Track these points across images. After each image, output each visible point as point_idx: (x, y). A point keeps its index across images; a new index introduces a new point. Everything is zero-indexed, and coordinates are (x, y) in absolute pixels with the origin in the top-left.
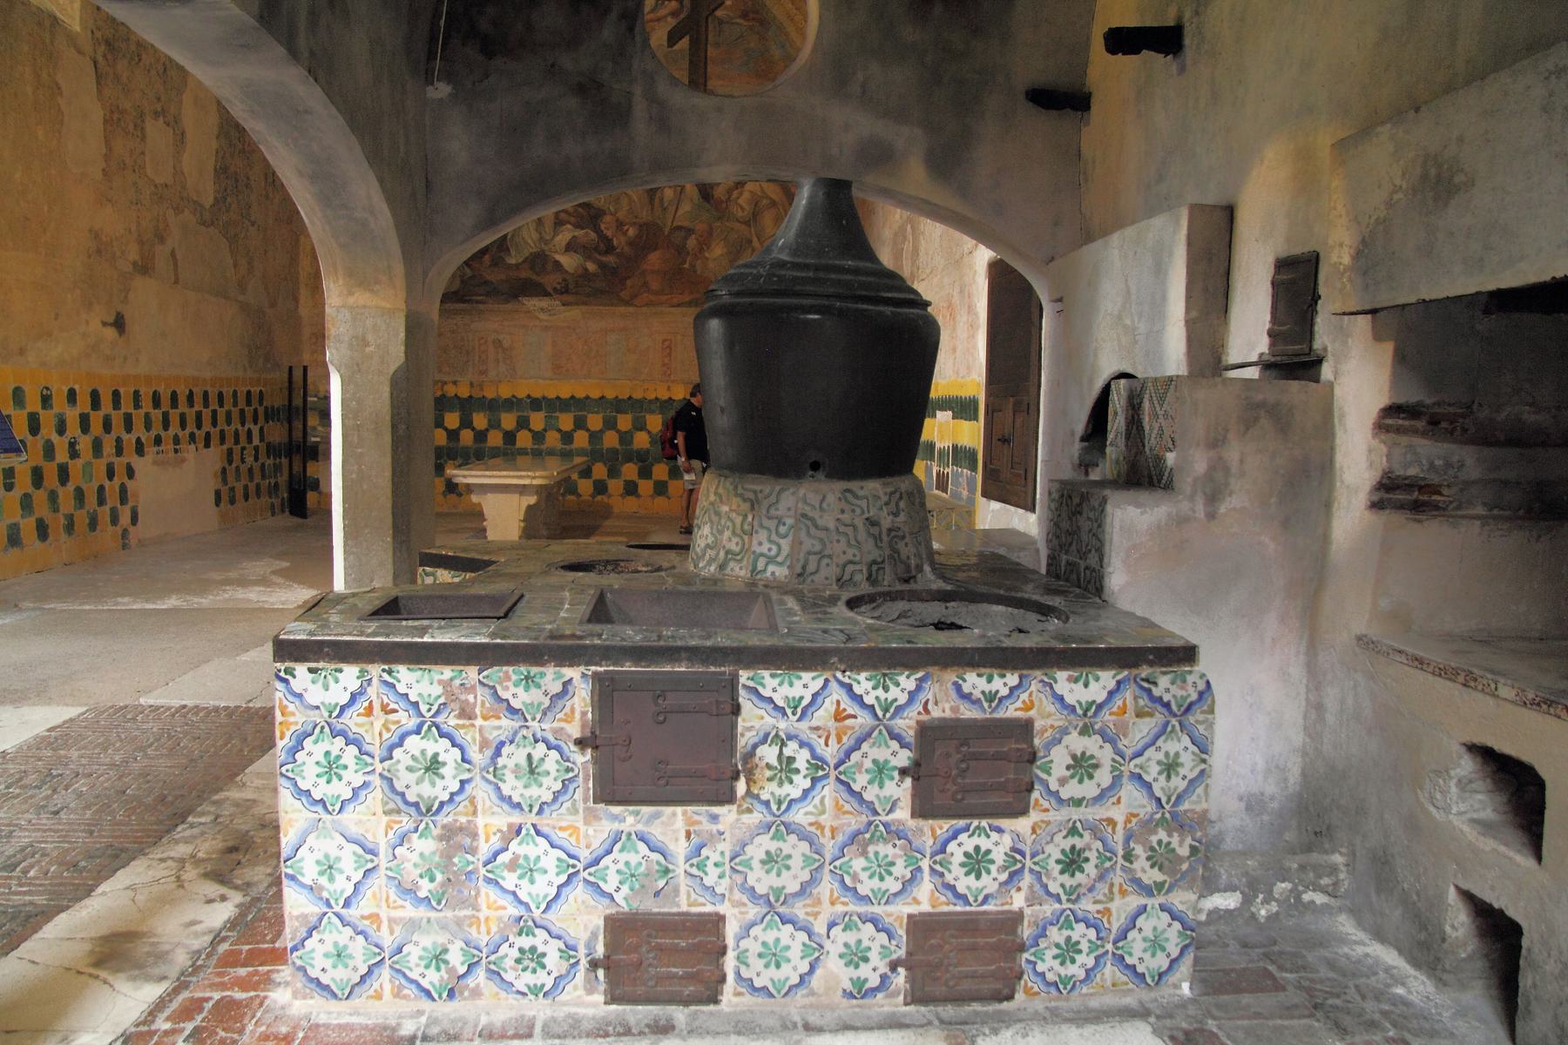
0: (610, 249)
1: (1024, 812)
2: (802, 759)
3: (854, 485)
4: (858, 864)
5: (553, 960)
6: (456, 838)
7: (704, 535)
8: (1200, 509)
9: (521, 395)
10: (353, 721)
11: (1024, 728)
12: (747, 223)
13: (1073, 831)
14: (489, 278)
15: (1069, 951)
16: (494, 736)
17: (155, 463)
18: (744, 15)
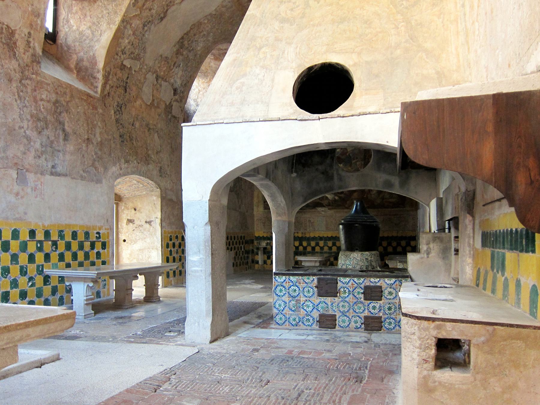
1: (381, 300)
2: (347, 291)
3: (363, 253)
4: (356, 307)
5: (311, 321)
6: (298, 301)
7: (339, 261)
8: (425, 256)
9: (317, 236)
10: (284, 284)
11: (381, 287)
13: (389, 304)
15: (390, 323)
16: (304, 286)
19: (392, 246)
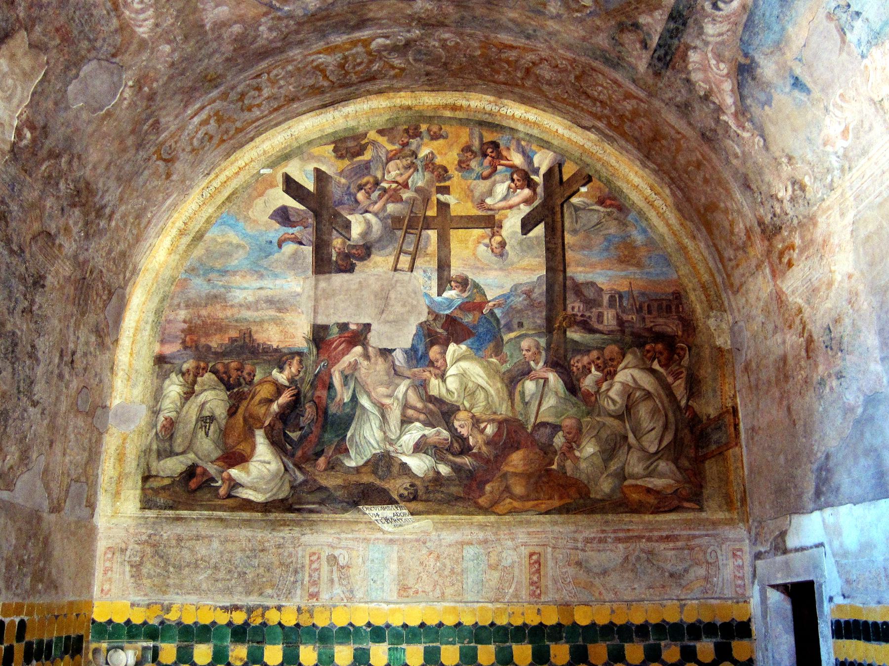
0: (465, 449)
9: (360, 622)
12: (620, 417)
14: (324, 482)
18: (601, 202)
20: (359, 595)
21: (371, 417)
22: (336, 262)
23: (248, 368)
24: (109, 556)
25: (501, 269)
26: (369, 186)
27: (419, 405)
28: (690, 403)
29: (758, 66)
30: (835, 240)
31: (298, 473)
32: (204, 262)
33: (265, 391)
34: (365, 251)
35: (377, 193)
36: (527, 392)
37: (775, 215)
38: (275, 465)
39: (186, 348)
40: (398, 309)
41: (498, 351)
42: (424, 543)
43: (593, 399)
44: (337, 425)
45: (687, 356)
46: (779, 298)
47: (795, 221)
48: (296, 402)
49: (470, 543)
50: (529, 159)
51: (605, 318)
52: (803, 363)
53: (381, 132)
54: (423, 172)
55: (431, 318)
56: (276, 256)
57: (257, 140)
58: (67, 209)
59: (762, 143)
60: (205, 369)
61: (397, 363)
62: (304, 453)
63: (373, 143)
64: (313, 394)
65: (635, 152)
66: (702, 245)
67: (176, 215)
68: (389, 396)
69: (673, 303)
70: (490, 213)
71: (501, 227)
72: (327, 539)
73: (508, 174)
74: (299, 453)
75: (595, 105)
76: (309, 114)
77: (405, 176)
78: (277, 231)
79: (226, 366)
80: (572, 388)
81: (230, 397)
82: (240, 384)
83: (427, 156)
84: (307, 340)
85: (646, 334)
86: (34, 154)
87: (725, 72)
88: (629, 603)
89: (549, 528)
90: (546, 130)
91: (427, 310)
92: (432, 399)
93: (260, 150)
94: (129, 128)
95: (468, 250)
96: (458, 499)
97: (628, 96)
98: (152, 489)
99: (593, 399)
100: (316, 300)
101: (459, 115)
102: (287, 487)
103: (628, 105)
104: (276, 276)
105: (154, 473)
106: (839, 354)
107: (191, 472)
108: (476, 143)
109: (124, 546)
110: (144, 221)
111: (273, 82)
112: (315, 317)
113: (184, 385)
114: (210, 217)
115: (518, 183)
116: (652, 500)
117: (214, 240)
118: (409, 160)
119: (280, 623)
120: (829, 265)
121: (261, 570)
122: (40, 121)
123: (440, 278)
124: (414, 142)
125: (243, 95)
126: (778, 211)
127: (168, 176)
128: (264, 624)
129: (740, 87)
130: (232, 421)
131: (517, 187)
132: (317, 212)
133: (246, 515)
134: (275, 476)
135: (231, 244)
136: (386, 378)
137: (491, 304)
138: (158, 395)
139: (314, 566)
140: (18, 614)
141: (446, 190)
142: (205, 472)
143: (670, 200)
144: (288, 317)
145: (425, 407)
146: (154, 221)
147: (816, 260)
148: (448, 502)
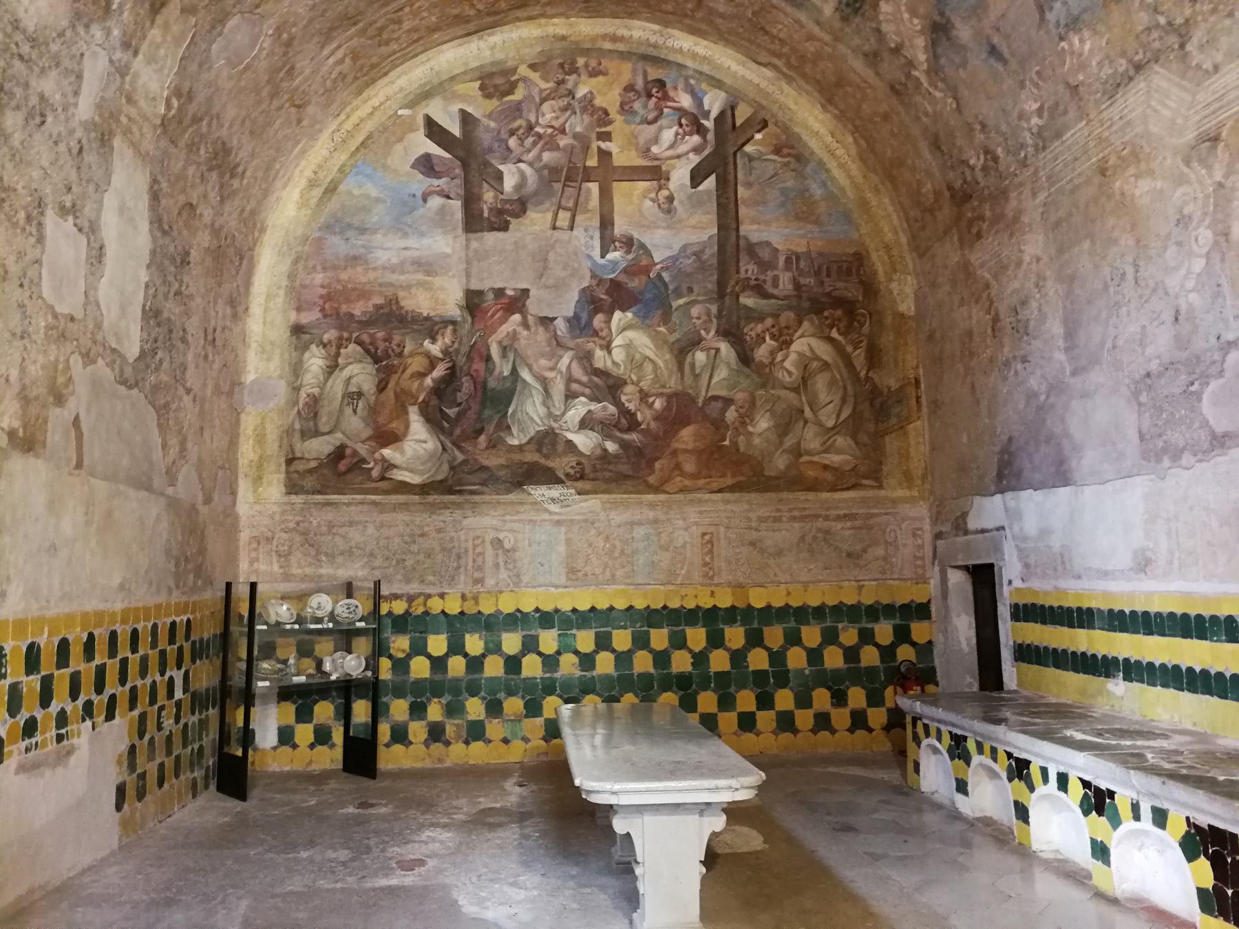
0: (633, 425)
9: (528, 608)
12: (796, 390)
14: (486, 463)
17: (22, 769)
18: (777, 151)
19: (840, 645)
20: (525, 579)
21: (534, 392)
22: (488, 219)
23: (397, 338)
24: (255, 545)
25: (668, 227)
26: (521, 131)
27: (584, 379)
28: (870, 374)
29: (953, 27)
30: (1025, 219)
31: (457, 453)
32: (336, 220)
33: (417, 364)
34: (520, 206)
35: (531, 139)
36: (697, 364)
37: (965, 182)
38: (432, 444)
39: (325, 316)
40: (558, 272)
41: (666, 319)
42: (593, 523)
43: (767, 370)
44: (498, 399)
45: (868, 323)
46: (966, 269)
47: (986, 192)
48: (452, 376)
49: (640, 523)
50: (699, 102)
51: (781, 282)
52: (988, 341)
53: (533, 67)
54: (582, 114)
55: (594, 283)
56: (421, 211)
57: (392, 74)
58: (206, 174)
59: (954, 106)
60: (349, 340)
61: (559, 333)
62: (463, 431)
63: (524, 79)
64: (469, 368)
65: (816, 94)
66: (886, 200)
67: (303, 163)
68: (552, 369)
69: (854, 265)
70: (656, 163)
71: (668, 179)
72: (486, 520)
73: (676, 118)
74: (458, 431)
75: (773, 42)
76: (449, 44)
77: (561, 120)
78: (420, 183)
79: (372, 336)
80: (745, 358)
81: (378, 370)
82: (388, 357)
83: (585, 96)
84: (461, 308)
85: (824, 300)
86: (180, 122)
87: (919, 27)
88: (806, 585)
89: (722, 507)
90: (718, 66)
91: (589, 274)
92: (598, 372)
93: (396, 87)
94: (266, 78)
95: (633, 204)
96: (627, 477)
97: (811, 37)
98: (297, 472)
99: (767, 370)
100: (468, 262)
101: (621, 47)
102: (446, 467)
103: (810, 47)
104: (422, 235)
105: (298, 455)
106: (1025, 338)
107: (339, 453)
108: (640, 83)
109: (270, 534)
110: (273, 173)
111: (415, 14)
112: (468, 281)
113: (326, 358)
114: (344, 165)
115: (687, 129)
116: (829, 476)
117: (349, 193)
118: (565, 101)
119: (443, 612)
120: (1019, 243)
121: (421, 557)
122: (186, 86)
123: (602, 238)
124: (572, 79)
125: (382, 29)
126: (969, 178)
127: (299, 121)
128: (426, 613)
129: (933, 45)
130: (383, 397)
131: (685, 134)
132: (463, 158)
133: (401, 498)
134: (432, 456)
135: (368, 197)
136: (548, 349)
137: (658, 267)
138: (297, 369)
139: (479, 550)
140: (185, 613)
141: (607, 137)
142: (355, 453)
143: (853, 150)
144: (438, 281)
145: (590, 380)
146: (282, 172)
147: (1006, 236)
148: (616, 481)
